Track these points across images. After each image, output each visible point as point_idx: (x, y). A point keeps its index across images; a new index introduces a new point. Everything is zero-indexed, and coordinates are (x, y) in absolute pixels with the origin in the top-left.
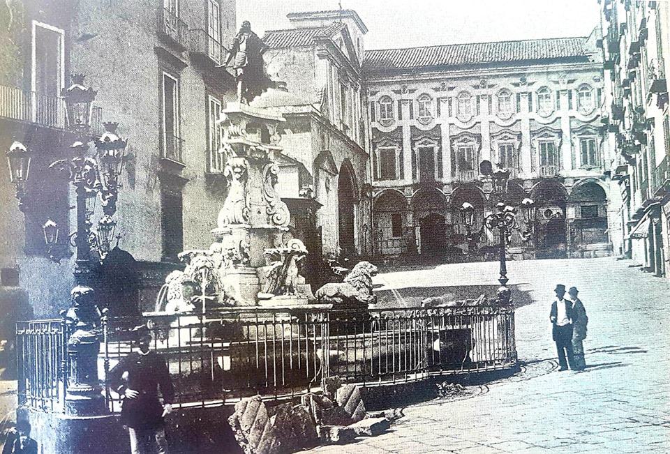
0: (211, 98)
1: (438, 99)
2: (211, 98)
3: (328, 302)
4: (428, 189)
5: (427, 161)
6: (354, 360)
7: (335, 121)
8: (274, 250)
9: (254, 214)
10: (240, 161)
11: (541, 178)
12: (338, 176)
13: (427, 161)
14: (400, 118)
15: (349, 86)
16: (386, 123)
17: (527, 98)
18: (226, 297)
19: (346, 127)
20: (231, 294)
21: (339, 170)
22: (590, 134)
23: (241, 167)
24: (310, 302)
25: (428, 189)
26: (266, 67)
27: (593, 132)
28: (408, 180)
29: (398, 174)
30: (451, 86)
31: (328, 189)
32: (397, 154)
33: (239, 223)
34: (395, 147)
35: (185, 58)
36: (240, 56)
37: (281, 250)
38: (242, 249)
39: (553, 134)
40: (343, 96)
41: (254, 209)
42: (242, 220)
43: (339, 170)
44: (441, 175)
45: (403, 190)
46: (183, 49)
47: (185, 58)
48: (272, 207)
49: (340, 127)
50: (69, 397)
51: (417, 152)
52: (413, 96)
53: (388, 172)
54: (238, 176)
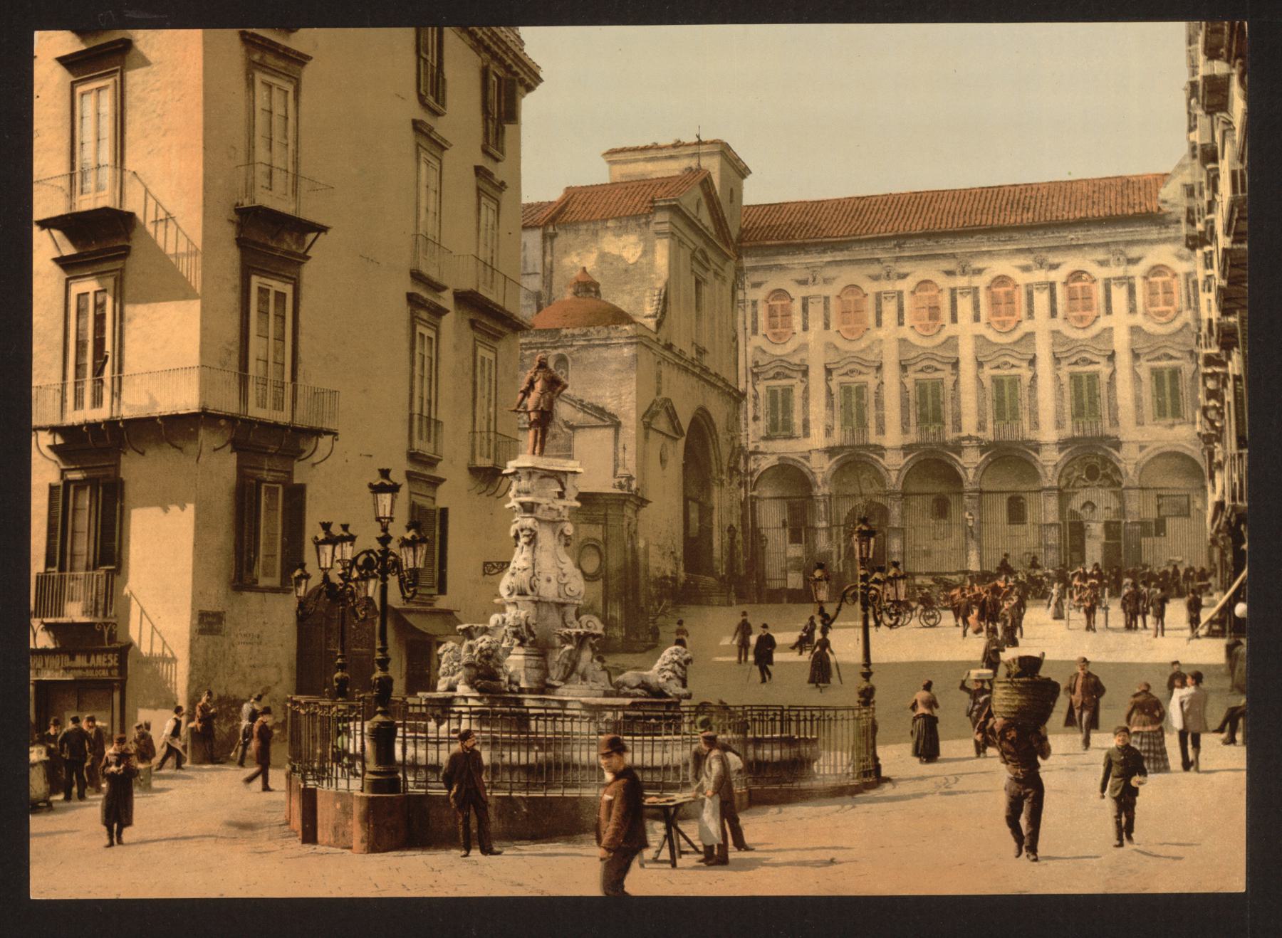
0: (481, 352)
2: (481, 352)
4: (855, 460)
5: (853, 404)
6: (649, 764)
8: (567, 631)
10: (529, 522)
12: (684, 439)
14: (805, 328)
16: (778, 338)
18: (510, 682)
19: (701, 351)
20: (515, 678)
21: (685, 428)
22: (1171, 358)
23: (531, 530)
25: (855, 460)
26: (566, 661)
27: (1179, 355)
28: (818, 439)
29: (798, 430)
31: (663, 461)
34: (793, 382)
35: (446, 299)
36: (534, 395)
38: (528, 626)
39: (1096, 359)
42: (529, 592)
44: (881, 430)
45: (807, 458)
46: (444, 288)
49: (690, 353)
53: (780, 427)
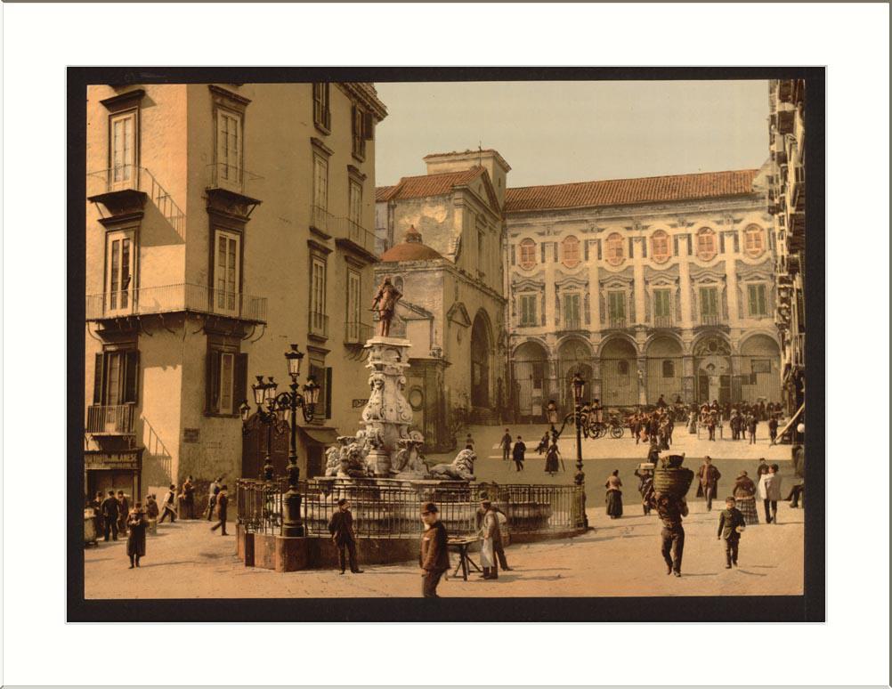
0: (352, 275)
1: (586, 242)
3: (438, 478)
5: (571, 306)
7: (470, 270)
8: (402, 440)
9: (388, 412)
10: (380, 376)
11: (702, 327)
13: (571, 306)
15: (487, 230)
16: (527, 267)
17: (686, 240)
19: (482, 275)
21: (472, 320)
22: (760, 279)
24: (426, 478)
25: (572, 339)
27: (764, 277)
29: (539, 322)
30: (601, 227)
32: (539, 299)
33: (378, 419)
35: (331, 245)
36: (383, 301)
37: (406, 441)
38: (379, 437)
40: (480, 241)
41: (388, 409)
43: (472, 320)
44: (588, 322)
45: (544, 338)
47: (331, 245)
48: (401, 407)
49: (475, 276)
50: (284, 526)
51: (561, 297)
52: (559, 239)
53: (528, 320)
54: (378, 386)
